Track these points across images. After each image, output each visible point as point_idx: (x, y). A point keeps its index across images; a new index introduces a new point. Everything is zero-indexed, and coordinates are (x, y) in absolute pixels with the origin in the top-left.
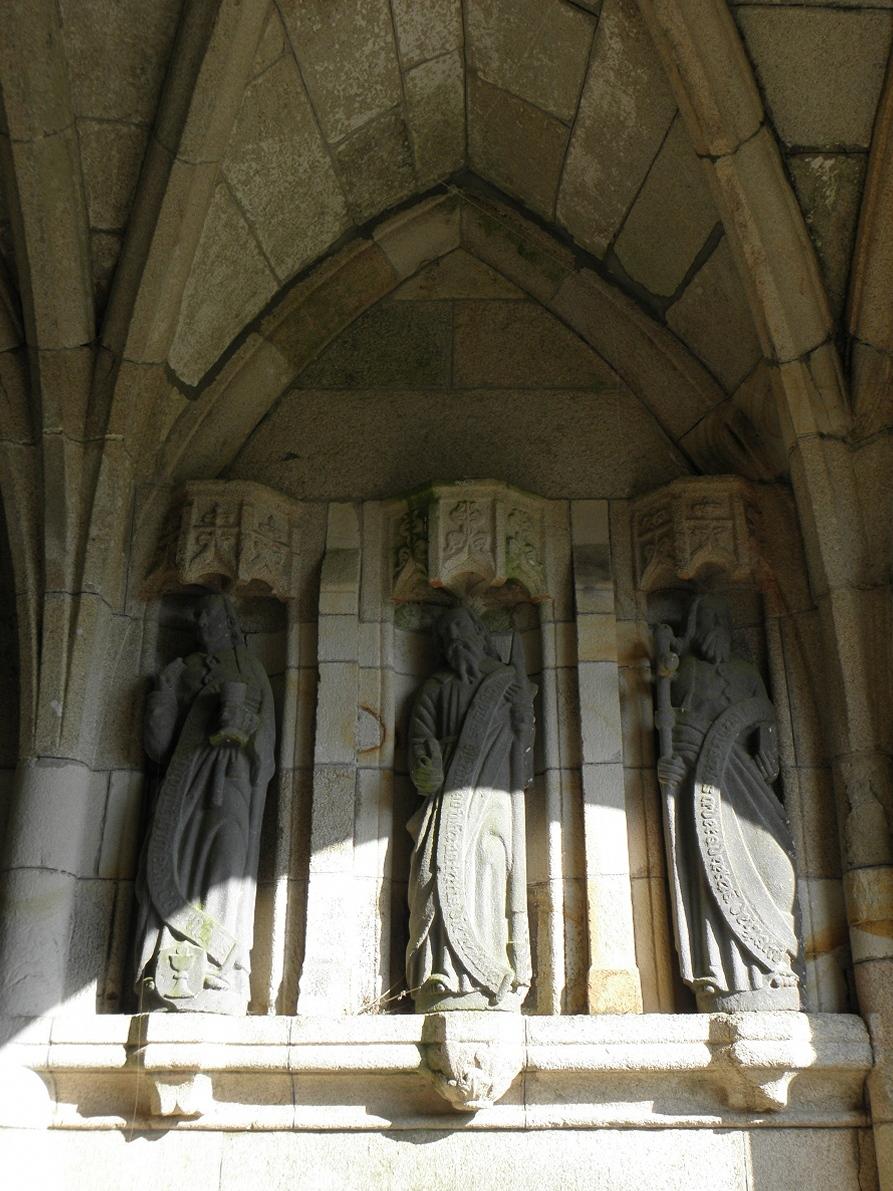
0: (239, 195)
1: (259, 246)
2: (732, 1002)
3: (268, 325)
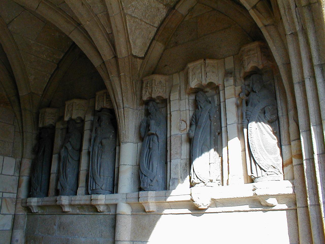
0: (133, 15)
1: (145, 22)
2: (257, 180)
3: (157, 37)
